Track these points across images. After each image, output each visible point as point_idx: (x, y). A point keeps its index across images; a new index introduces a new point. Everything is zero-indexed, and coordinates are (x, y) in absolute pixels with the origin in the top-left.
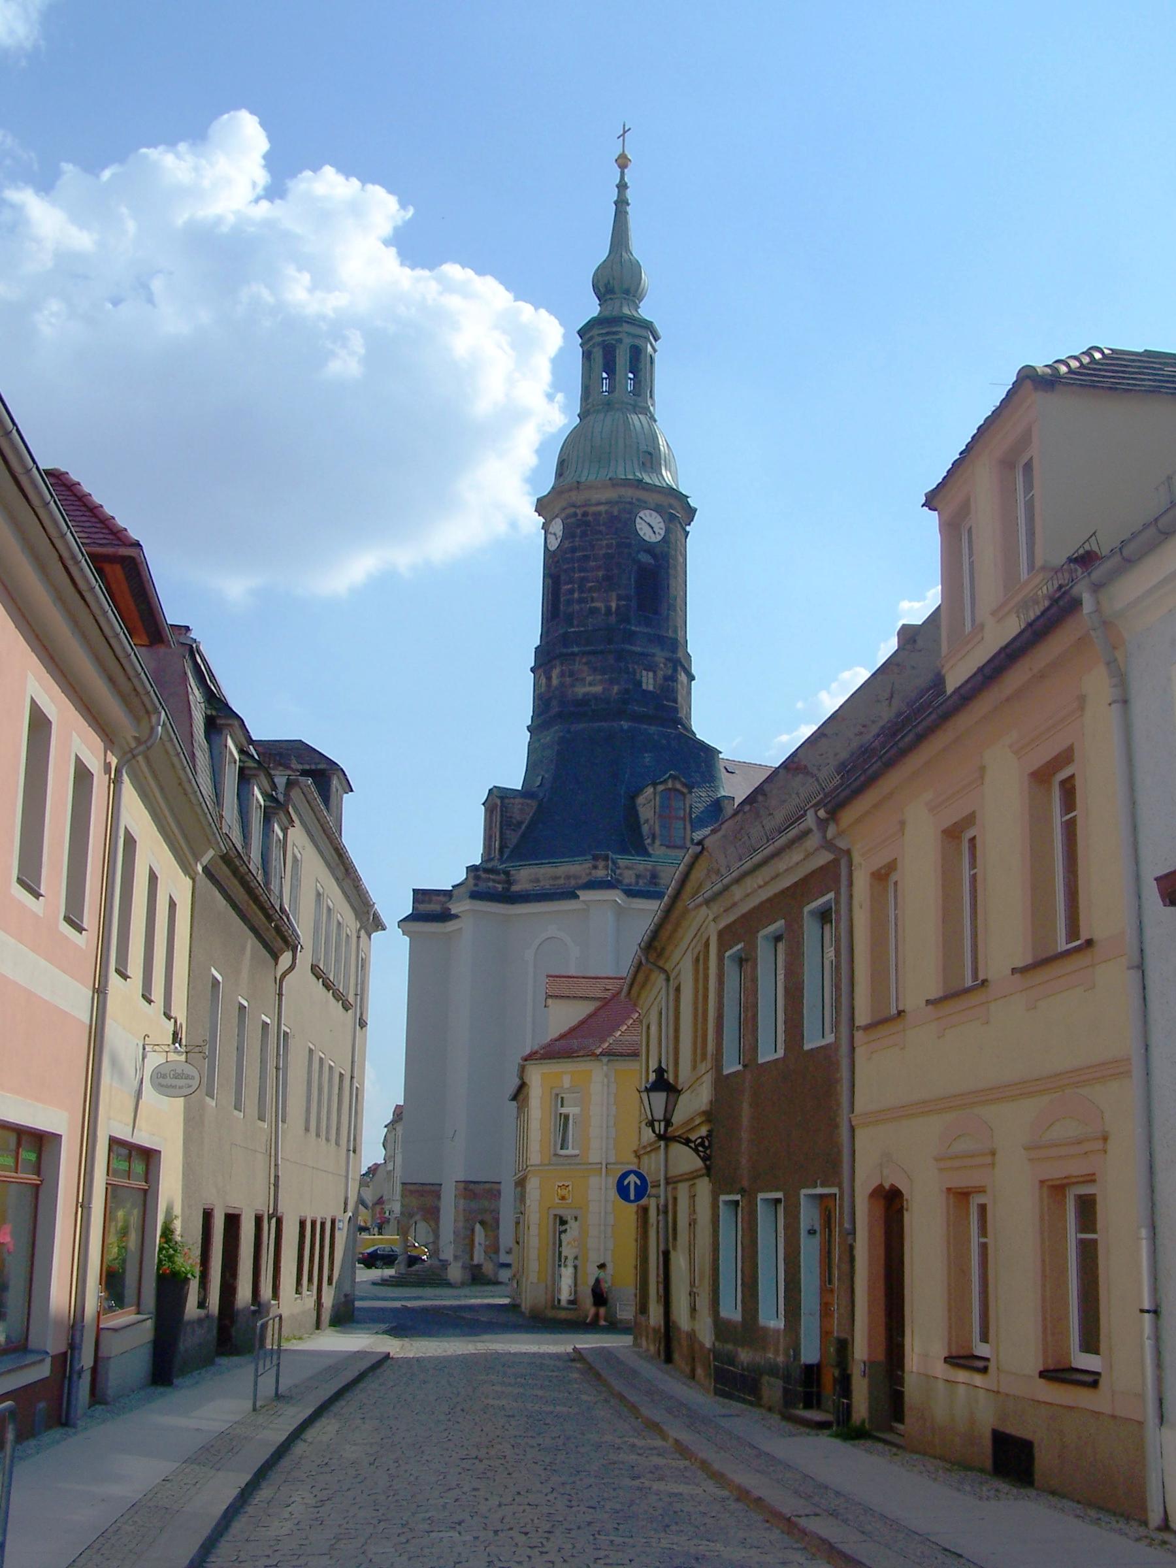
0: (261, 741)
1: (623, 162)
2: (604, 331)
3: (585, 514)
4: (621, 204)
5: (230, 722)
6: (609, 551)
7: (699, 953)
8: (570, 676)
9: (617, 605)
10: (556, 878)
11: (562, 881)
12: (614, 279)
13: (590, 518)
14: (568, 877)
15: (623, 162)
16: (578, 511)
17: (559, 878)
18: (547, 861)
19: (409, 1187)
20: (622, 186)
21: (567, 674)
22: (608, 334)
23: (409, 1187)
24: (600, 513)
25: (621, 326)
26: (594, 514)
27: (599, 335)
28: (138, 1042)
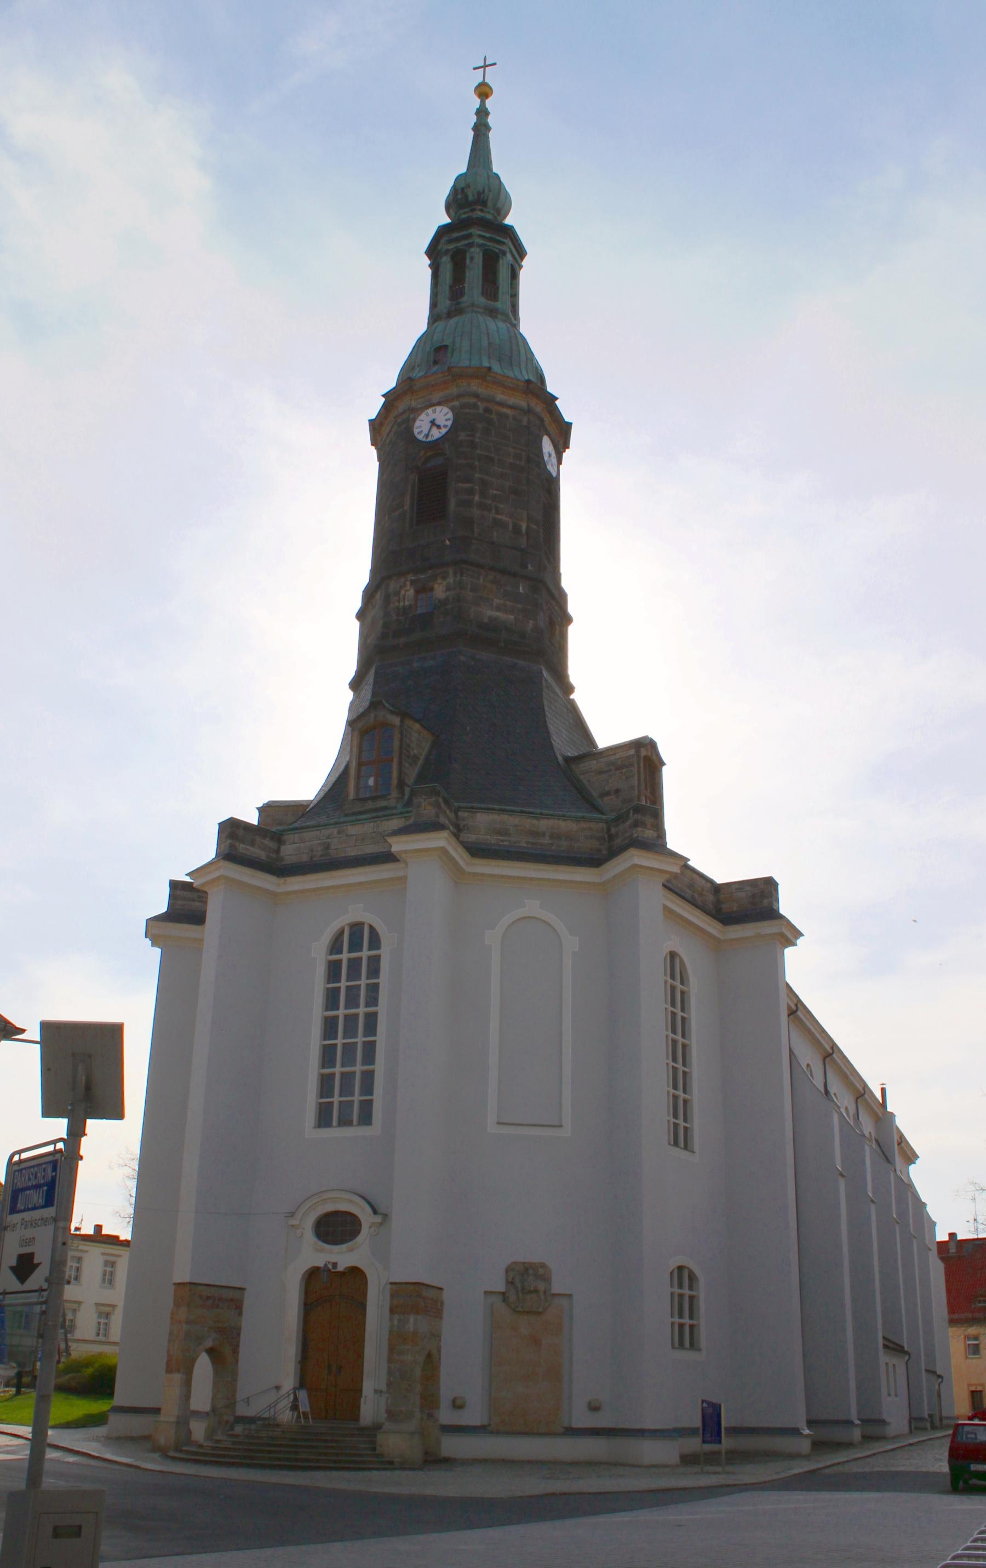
0: (526, 340)
1: (483, 91)
2: (487, 235)
3: (487, 410)
4: (481, 130)
5: (505, 241)
6: (518, 463)
7: (666, 956)
8: (472, 590)
9: (528, 527)
10: (535, 833)
11: (546, 841)
12: (490, 190)
13: (494, 417)
14: (556, 836)
15: (483, 91)
16: (479, 403)
17: (543, 835)
18: (519, 809)
19: (102, 1308)
20: (482, 113)
21: (469, 586)
22: (490, 239)
23: (102, 1308)
24: (507, 417)
25: (506, 238)
26: (500, 415)
27: (480, 236)
28: (666, 1006)
